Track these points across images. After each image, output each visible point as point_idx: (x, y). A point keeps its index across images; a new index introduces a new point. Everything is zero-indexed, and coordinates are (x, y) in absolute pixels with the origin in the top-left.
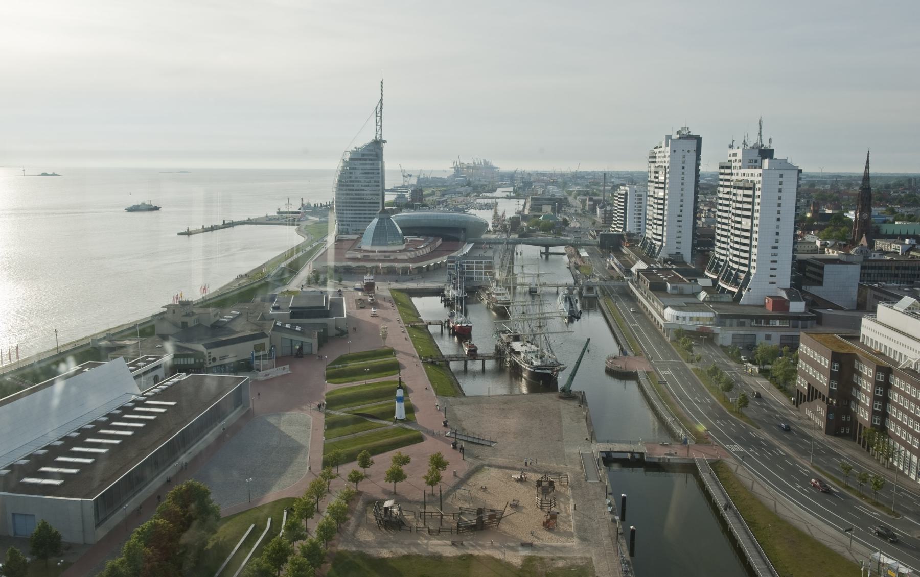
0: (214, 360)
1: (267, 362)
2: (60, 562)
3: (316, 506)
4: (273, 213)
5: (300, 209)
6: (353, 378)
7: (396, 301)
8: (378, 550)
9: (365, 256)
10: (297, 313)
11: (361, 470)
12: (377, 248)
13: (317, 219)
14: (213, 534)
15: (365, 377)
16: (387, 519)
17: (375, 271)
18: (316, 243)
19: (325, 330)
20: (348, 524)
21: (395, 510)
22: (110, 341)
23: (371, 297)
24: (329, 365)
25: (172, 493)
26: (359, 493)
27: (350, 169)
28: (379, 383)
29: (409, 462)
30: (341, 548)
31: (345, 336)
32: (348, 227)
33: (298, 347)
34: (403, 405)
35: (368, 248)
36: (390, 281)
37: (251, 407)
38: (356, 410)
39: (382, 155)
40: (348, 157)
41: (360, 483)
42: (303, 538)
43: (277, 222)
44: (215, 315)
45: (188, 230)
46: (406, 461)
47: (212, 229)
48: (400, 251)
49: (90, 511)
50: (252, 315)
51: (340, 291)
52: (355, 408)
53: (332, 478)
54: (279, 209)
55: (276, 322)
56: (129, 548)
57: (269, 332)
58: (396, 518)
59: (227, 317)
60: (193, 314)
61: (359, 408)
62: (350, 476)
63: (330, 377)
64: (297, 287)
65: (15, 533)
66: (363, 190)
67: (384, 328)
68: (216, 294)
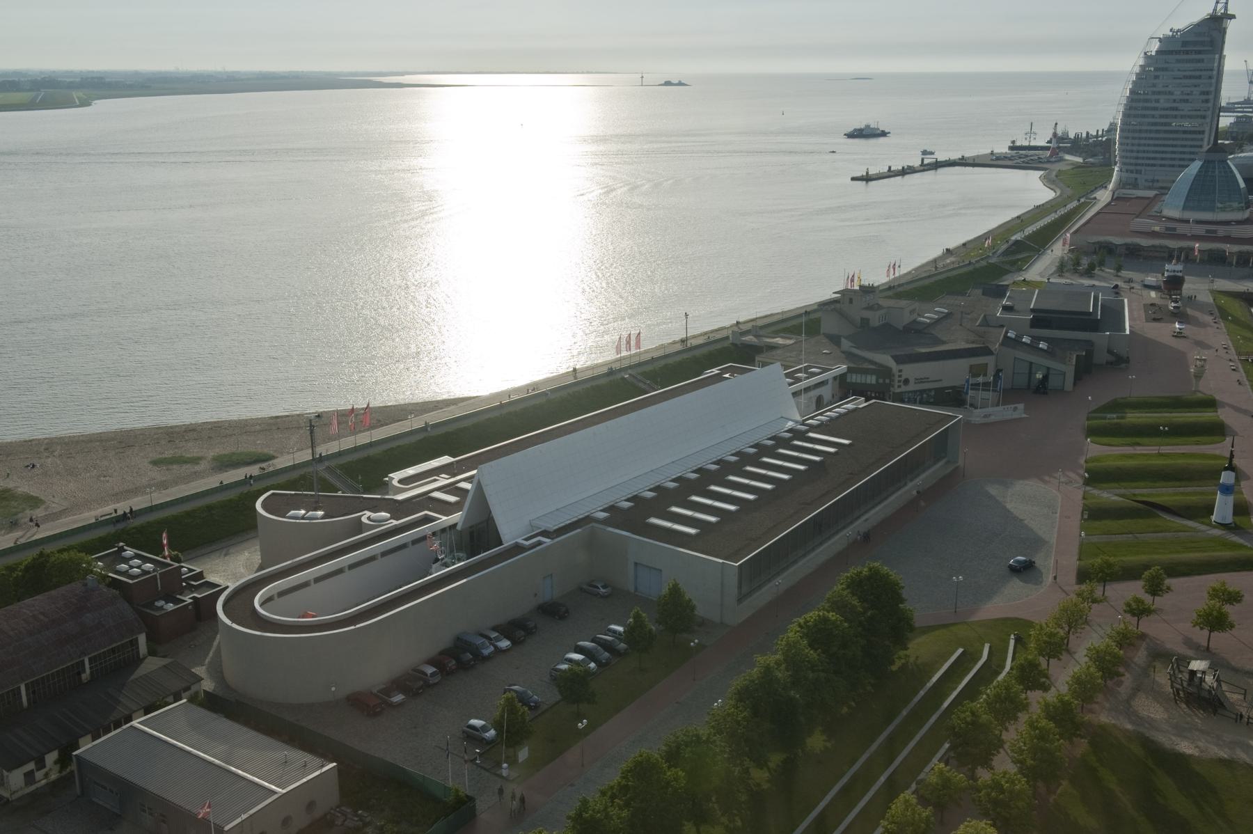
0: (906, 382)
1: (990, 395)
2: (694, 642)
3: (1066, 641)
4: (1002, 148)
5: (1049, 142)
6: (1138, 440)
7: (1223, 314)
8: (1174, 738)
9: (1167, 229)
10: (1042, 319)
11: (1148, 598)
12: (1192, 216)
13: (1080, 160)
14: (902, 649)
15: (1158, 440)
16: (1191, 689)
17: (1186, 256)
18: (1074, 204)
19: (1090, 354)
20: (1120, 684)
21: (1209, 679)
22: (756, 336)
23: (1176, 302)
24: (1094, 412)
25: (847, 577)
26: (1143, 636)
27: (1156, 70)
28: (1183, 454)
29: (1239, 601)
30: (1104, 718)
31: (1123, 365)
32: (1138, 176)
33: (1041, 376)
34: (1230, 499)
35: (1176, 214)
36: (1213, 277)
37: (961, 463)
38: (1140, 495)
39: (1223, 42)
40: (1155, 47)
41: (1144, 619)
42: (1045, 688)
43: (1010, 163)
44: (912, 312)
45: (867, 173)
46: (1234, 598)
47: (904, 172)
48: (1239, 222)
49: (733, 580)
50: (969, 317)
51: (1116, 286)
52: (1137, 491)
53: (1095, 601)
54: (1013, 142)
55: (1007, 332)
56: (788, 644)
57: (995, 347)
58: (1209, 692)
59: (928, 317)
60: (880, 307)
61: (1146, 492)
62: (1128, 605)
63: (1093, 432)
64: (1041, 275)
65: (636, 589)
66: (1177, 109)
67: (1200, 360)
68: (909, 278)
